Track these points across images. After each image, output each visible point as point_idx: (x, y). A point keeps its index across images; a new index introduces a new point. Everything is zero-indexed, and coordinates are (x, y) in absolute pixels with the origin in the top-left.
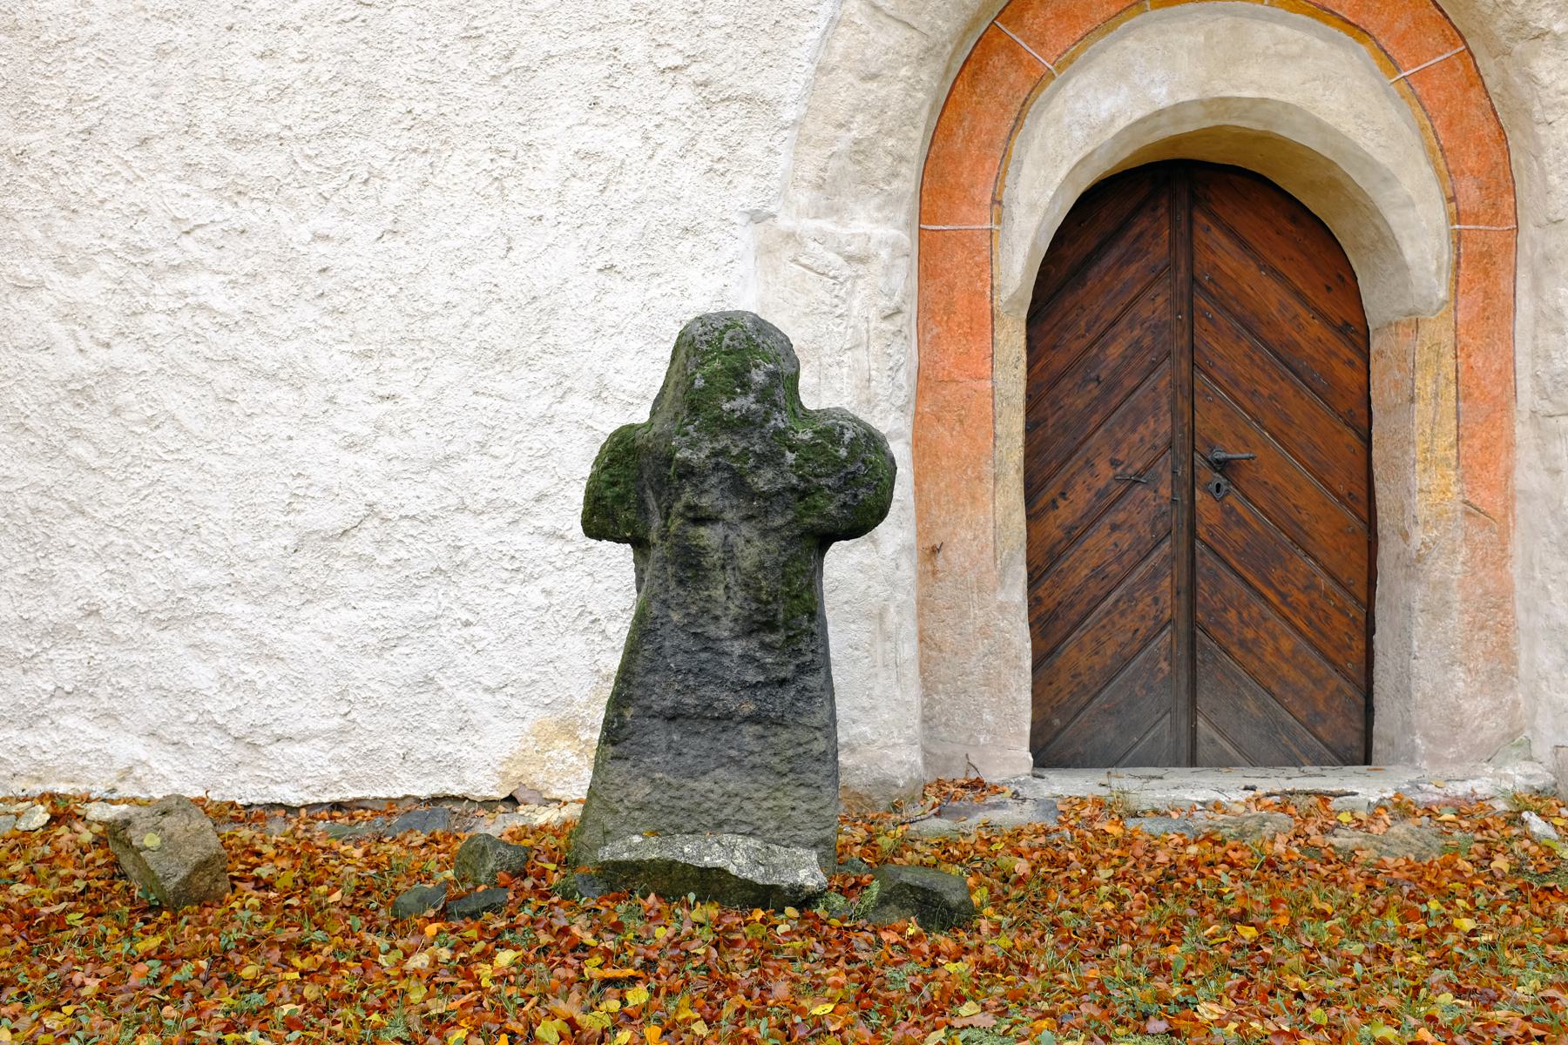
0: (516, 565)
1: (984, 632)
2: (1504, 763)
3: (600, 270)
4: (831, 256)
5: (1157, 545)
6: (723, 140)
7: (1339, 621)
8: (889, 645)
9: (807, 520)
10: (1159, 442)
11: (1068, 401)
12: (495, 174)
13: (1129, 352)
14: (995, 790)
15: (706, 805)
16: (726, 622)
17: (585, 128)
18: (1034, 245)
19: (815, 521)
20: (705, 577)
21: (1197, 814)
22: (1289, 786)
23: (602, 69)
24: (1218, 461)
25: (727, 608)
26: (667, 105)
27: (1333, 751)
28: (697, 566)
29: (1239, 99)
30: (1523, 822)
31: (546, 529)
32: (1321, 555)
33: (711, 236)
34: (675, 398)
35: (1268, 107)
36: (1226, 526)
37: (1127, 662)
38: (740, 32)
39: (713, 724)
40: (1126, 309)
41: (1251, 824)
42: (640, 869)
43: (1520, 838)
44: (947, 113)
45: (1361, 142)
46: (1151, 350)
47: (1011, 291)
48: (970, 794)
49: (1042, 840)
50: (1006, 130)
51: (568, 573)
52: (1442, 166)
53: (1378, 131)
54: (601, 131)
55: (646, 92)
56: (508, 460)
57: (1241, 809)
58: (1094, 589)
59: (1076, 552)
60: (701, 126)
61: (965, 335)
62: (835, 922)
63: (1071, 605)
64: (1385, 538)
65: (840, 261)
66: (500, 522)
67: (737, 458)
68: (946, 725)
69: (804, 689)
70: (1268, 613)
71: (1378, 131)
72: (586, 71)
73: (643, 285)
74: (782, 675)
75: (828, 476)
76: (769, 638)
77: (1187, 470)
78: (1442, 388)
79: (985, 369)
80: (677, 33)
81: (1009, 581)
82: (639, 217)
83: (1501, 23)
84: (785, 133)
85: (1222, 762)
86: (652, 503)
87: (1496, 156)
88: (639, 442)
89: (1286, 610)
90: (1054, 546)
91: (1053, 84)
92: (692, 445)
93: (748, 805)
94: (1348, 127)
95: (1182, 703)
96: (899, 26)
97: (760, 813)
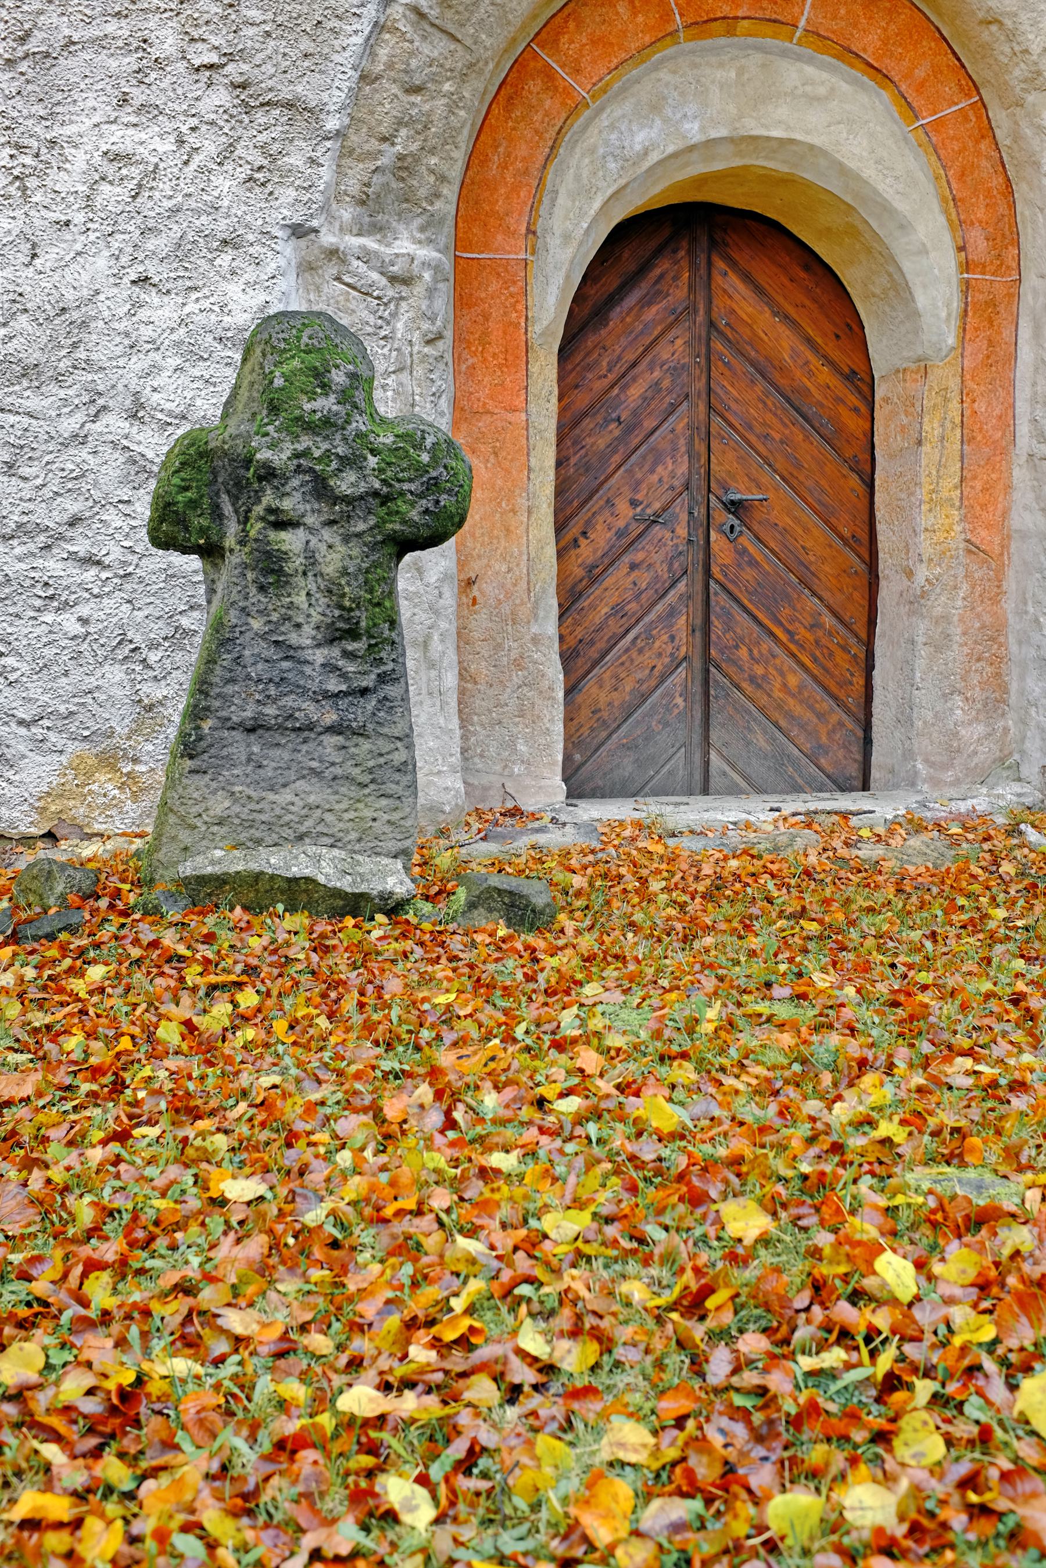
0: (51, 592)
1: (518, 664)
2: (997, 784)
3: (133, 282)
4: (375, 276)
5: (672, 585)
6: (263, 147)
7: (840, 657)
8: (433, 673)
9: (389, 526)
10: (676, 483)
11: (589, 441)
12: (16, 172)
13: (649, 394)
14: (534, 817)
15: (288, 818)
16: (308, 630)
17: (114, 127)
18: (568, 277)
19: (397, 527)
20: (287, 583)
21: (730, 833)
22: (812, 806)
23: (130, 62)
24: (732, 502)
25: (309, 616)
26: (203, 107)
27: (834, 782)
28: (280, 572)
29: (768, 139)
30: (1021, 833)
31: (81, 554)
32: (826, 595)
33: (251, 250)
34: (252, 399)
35: (794, 148)
36: (739, 565)
37: (644, 698)
38: (279, 32)
39: (293, 735)
40: (647, 349)
41: (783, 840)
42: (225, 882)
43: (1020, 846)
44: (482, 138)
45: (881, 187)
46: (670, 391)
47: (545, 323)
48: (509, 821)
49: (591, 858)
50: (541, 159)
51: (105, 601)
52: (954, 216)
53: (897, 178)
54: (131, 131)
55: (180, 91)
56: (39, 482)
57: (771, 828)
58: (615, 627)
59: (596, 591)
60: (240, 131)
61: (500, 366)
62: (427, 926)
63: (592, 643)
64: (887, 578)
65: (384, 281)
66: (32, 547)
67: (319, 460)
68: (482, 756)
69: (385, 698)
70: (777, 650)
71: (897, 178)
72: (113, 63)
73: (180, 300)
74: (364, 684)
75: (411, 480)
76: (351, 646)
77: (703, 511)
78: (948, 431)
79: (519, 402)
80: (213, 27)
81: (541, 614)
82: (175, 227)
83: (1017, 72)
84: (328, 144)
85: (733, 791)
86: (228, 509)
87: (1003, 209)
88: (212, 445)
89: (792, 647)
90: (575, 585)
91: (587, 113)
92: (272, 446)
93: (329, 817)
94: (869, 172)
95: (697, 738)
96: (444, 36)
97: (341, 825)
